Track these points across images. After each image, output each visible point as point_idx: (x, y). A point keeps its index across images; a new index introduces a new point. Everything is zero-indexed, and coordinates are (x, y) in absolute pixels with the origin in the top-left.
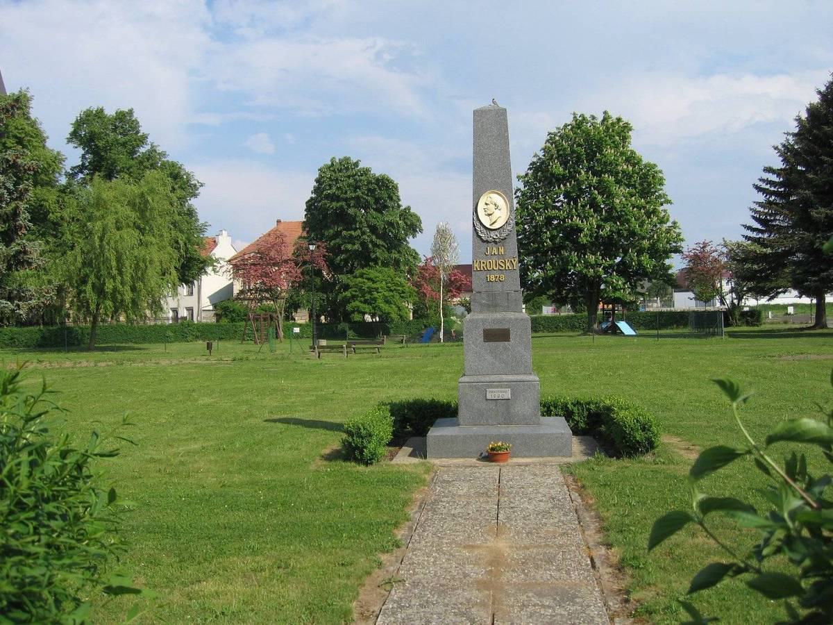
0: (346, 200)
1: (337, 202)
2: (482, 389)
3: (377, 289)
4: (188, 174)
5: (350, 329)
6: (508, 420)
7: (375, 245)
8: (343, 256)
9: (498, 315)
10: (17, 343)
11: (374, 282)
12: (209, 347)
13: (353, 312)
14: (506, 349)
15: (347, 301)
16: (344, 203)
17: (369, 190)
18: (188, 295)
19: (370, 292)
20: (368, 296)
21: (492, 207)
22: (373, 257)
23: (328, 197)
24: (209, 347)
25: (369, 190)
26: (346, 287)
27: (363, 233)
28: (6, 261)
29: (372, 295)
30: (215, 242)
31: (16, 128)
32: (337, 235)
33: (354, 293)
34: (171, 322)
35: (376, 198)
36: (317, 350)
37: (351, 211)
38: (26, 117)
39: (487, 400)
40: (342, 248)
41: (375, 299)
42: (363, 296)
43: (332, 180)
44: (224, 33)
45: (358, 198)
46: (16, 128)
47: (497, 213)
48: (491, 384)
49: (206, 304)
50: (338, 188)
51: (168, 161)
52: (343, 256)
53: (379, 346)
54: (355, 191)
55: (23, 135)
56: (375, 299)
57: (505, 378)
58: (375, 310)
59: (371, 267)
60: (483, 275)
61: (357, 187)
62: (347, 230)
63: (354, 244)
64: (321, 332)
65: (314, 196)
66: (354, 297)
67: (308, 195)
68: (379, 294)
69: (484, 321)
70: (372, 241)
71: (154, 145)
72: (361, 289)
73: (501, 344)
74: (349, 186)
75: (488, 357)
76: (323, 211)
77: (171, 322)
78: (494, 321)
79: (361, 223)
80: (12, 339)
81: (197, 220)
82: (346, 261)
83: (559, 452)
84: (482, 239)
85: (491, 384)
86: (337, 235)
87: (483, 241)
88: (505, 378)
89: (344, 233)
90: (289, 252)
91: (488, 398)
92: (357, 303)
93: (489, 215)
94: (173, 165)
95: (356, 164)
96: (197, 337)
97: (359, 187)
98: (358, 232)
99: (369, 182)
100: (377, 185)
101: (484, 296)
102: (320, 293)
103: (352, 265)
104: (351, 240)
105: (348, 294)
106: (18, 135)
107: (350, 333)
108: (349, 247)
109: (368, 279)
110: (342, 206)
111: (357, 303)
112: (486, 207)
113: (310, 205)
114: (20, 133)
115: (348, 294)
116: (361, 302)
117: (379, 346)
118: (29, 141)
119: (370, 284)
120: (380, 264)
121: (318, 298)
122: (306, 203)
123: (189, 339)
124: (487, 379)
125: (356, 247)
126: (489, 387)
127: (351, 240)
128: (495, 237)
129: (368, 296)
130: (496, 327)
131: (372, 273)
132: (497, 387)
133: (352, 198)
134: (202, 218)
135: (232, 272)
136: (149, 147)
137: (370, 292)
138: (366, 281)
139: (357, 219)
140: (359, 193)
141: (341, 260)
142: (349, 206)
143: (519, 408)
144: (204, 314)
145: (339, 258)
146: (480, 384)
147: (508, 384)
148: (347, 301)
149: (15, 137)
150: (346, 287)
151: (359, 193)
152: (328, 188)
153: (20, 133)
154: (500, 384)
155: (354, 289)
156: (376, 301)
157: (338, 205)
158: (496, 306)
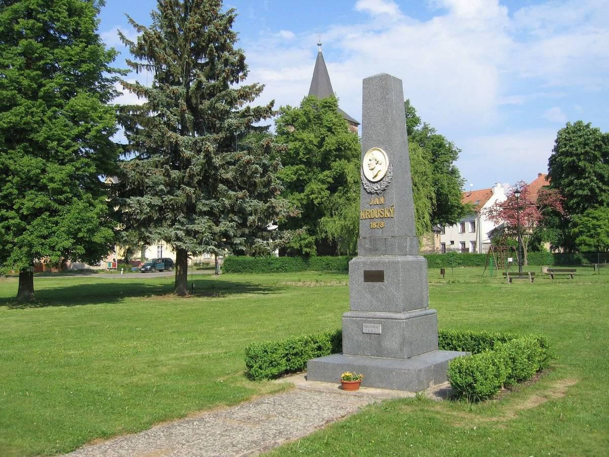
0: (578, 155)
1: (571, 158)
2: (359, 323)
3: (599, 226)
4: (450, 144)
5: (585, 258)
6: (380, 352)
7: (602, 190)
8: (575, 200)
9: (376, 259)
10: (331, 267)
11: (598, 220)
12: (443, 272)
13: (580, 244)
14: (381, 289)
15: (577, 235)
16: (575, 158)
17: (596, 146)
18: (473, 232)
19: (594, 229)
20: (593, 232)
21: (374, 162)
22: (600, 199)
23: (563, 154)
24: (443, 272)
25: (596, 146)
26: (575, 225)
27: (592, 181)
28: (262, 213)
29: (596, 230)
30: (491, 192)
31: (327, 121)
32: (571, 183)
33: (581, 229)
34: (460, 252)
35: (602, 152)
36: (508, 277)
37: (581, 164)
38: (334, 112)
39: (363, 333)
40: (575, 193)
41: (598, 234)
42: (589, 231)
43: (567, 140)
44: (522, 36)
45: (586, 153)
46: (327, 121)
47: (378, 167)
48: (367, 320)
49: (485, 238)
50: (572, 146)
51: (435, 135)
52: (575, 200)
53: (572, 273)
54: (584, 148)
55: (331, 125)
56: (598, 234)
57: (379, 314)
58: (598, 242)
59: (596, 208)
60: (367, 222)
61: (585, 144)
62: (578, 178)
63: (584, 190)
64: (559, 260)
65: (554, 153)
66: (581, 233)
67: (550, 153)
68: (602, 230)
69: (364, 263)
70: (598, 187)
71: (426, 124)
72: (586, 226)
73: (377, 284)
74: (579, 144)
75: (368, 296)
76: (560, 165)
77: (460, 252)
78: (372, 263)
79: (590, 173)
80: (328, 264)
81: (459, 177)
82: (578, 204)
83: (407, 387)
84: (367, 191)
85: (367, 320)
86: (571, 183)
87: (369, 193)
88: (379, 314)
89: (575, 181)
90: (533, 197)
91: (364, 332)
92: (584, 237)
93: (372, 169)
94: (439, 137)
95: (588, 126)
96: (459, 264)
97: (587, 144)
98: (588, 180)
99: (596, 140)
100: (603, 142)
101: (367, 241)
102: (558, 229)
103: (583, 206)
104: (582, 187)
105: (576, 230)
106: (328, 125)
107: (585, 261)
108: (580, 192)
109: (594, 218)
110: (574, 160)
111: (584, 237)
112: (369, 162)
113: (552, 161)
114: (329, 124)
115: (576, 230)
116: (587, 236)
117: (572, 273)
118: (335, 128)
119: (595, 222)
120: (605, 205)
121: (555, 233)
122: (549, 159)
123: (453, 265)
124: (364, 314)
125: (585, 192)
126: (365, 322)
127: (582, 187)
128: (376, 189)
129: (593, 232)
130: (373, 269)
131: (597, 213)
132: (370, 322)
133: (582, 154)
134: (462, 174)
135: (487, 215)
136: (422, 125)
137: (594, 229)
138: (591, 219)
139: (587, 170)
140: (587, 148)
141: (573, 204)
142: (580, 160)
143: (388, 343)
144: (483, 246)
145: (572, 202)
146: (369, 319)
147: (380, 320)
148: (577, 235)
149: (326, 126)
150: (575, 225)
151: (587, 148)
152: (563, 146)
153: (329, 124)
154: (374, 320)
155: (581, 226)
156: (599, 235)
157: (571, 159)
158: (377, 250)
